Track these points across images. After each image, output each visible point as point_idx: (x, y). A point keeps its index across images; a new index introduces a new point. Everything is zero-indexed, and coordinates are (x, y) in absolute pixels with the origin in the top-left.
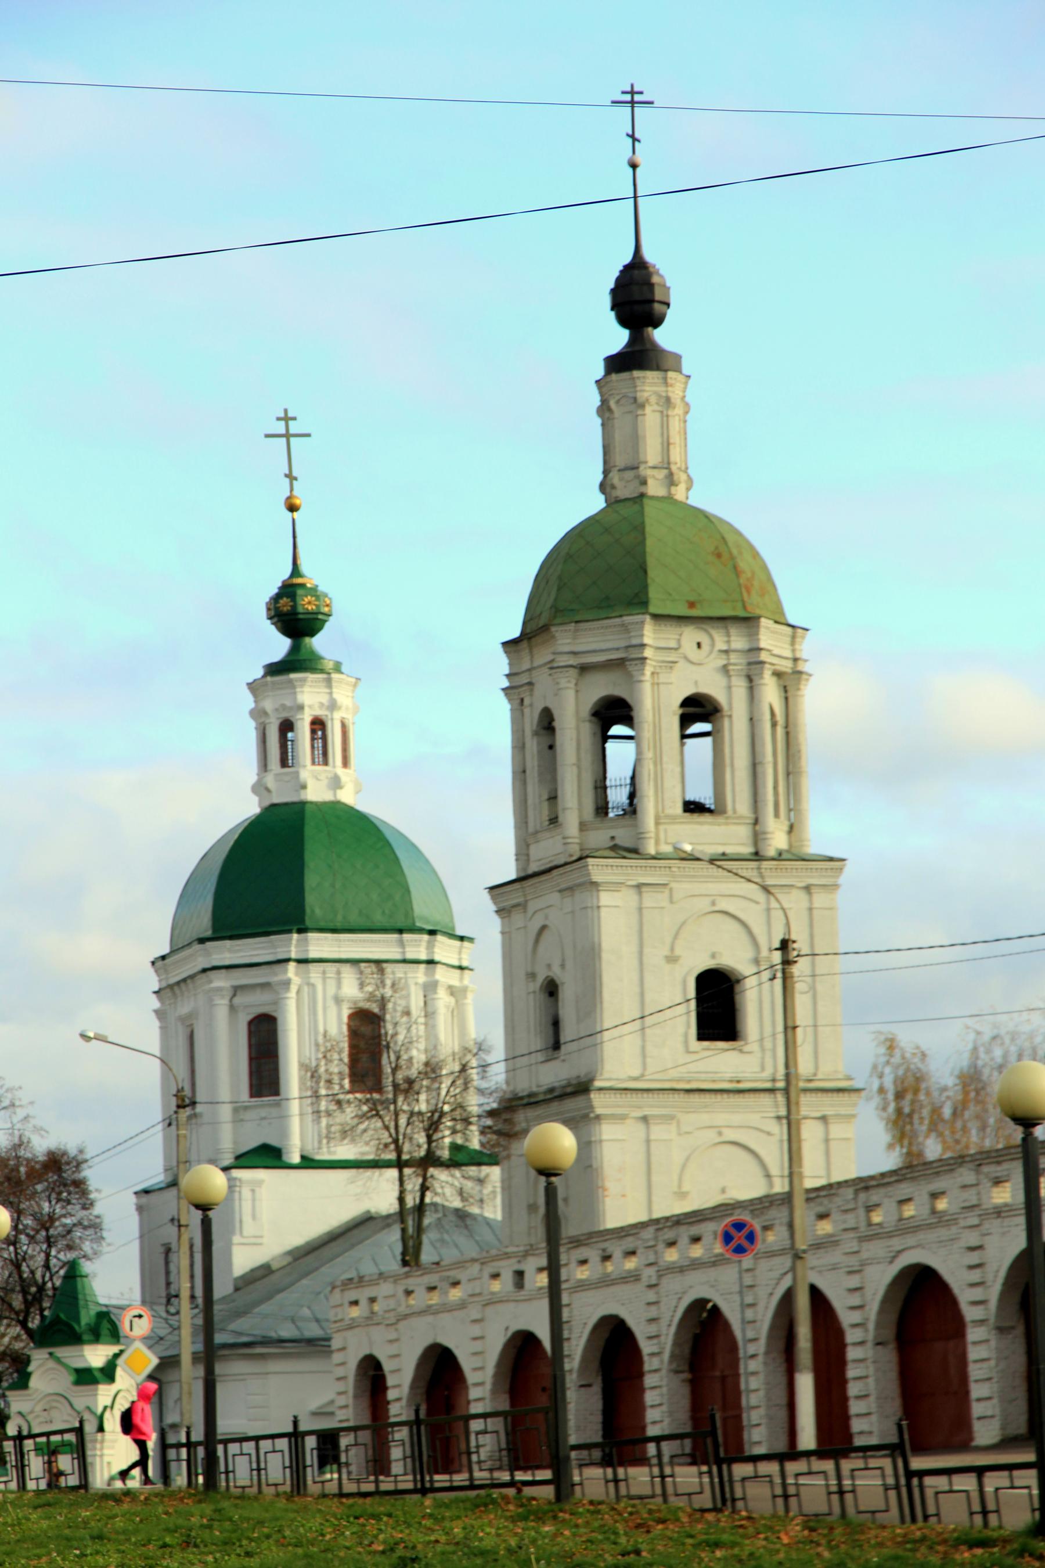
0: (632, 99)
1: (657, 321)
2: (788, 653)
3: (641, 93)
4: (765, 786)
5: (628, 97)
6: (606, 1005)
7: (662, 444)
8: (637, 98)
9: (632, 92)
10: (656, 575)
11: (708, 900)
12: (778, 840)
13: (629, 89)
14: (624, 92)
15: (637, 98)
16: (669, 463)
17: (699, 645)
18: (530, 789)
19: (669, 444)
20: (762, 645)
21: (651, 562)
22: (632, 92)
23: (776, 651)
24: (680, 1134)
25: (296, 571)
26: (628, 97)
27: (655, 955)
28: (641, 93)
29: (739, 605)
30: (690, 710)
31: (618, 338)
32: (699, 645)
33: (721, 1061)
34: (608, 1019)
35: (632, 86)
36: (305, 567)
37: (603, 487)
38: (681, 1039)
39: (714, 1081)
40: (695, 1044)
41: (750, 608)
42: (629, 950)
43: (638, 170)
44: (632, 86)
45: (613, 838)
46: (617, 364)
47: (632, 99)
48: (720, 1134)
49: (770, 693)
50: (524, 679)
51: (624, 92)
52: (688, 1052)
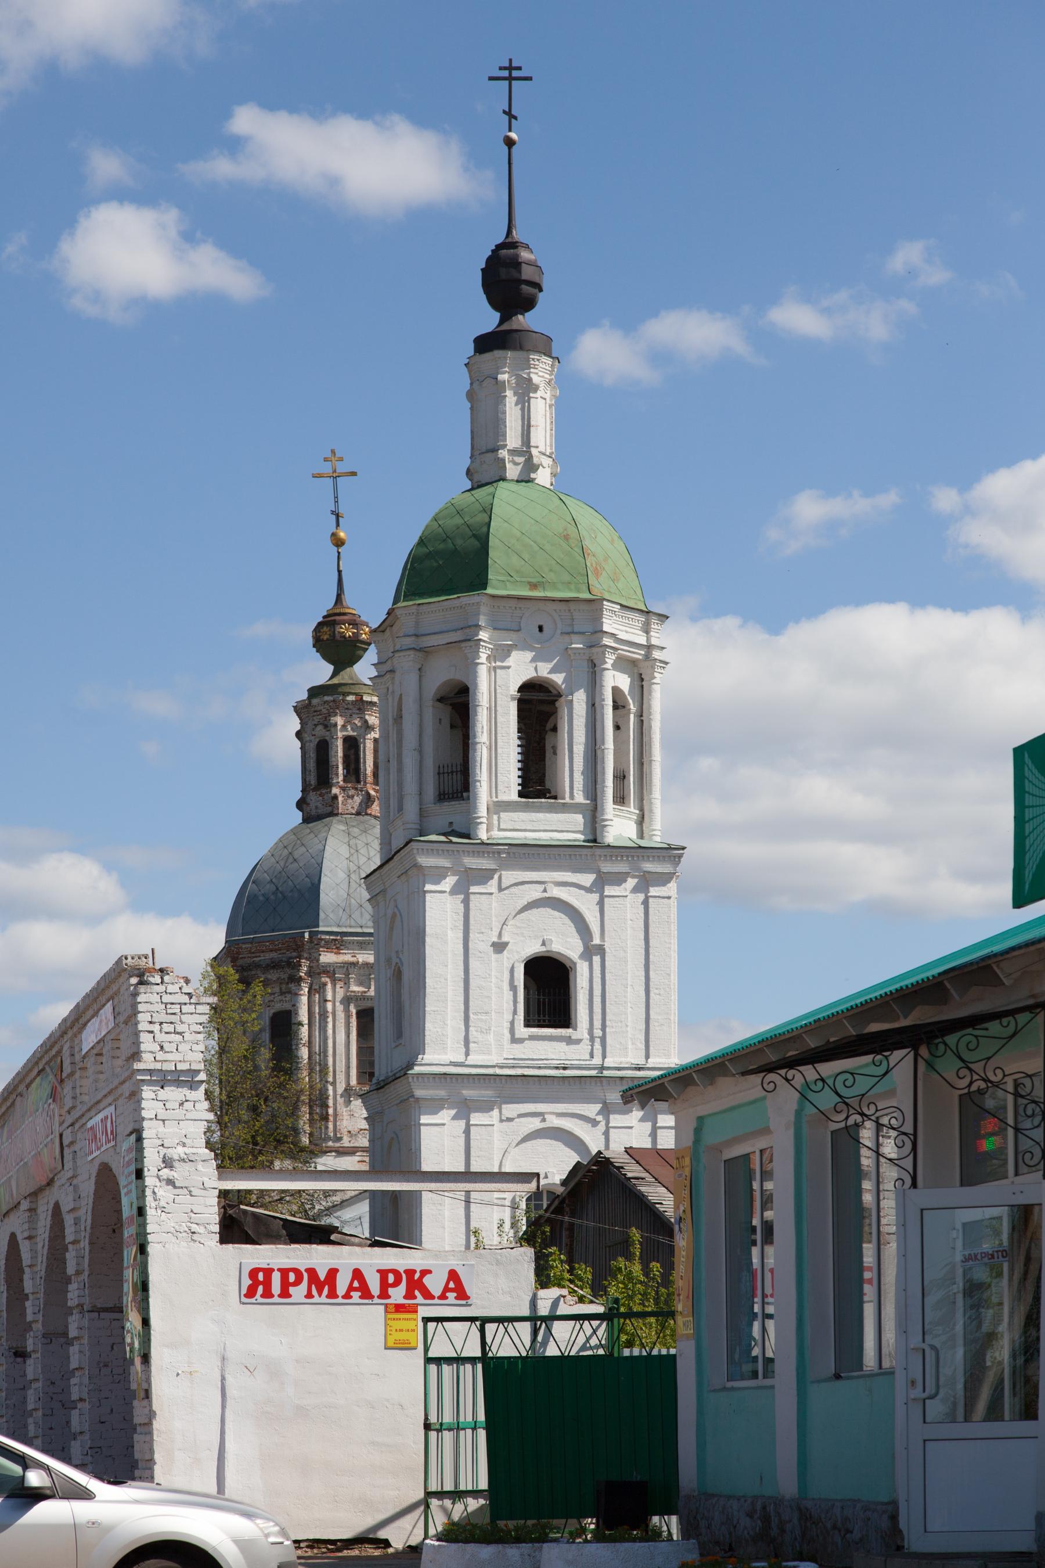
0: (511, 74)
1: (529, 304)
2: (642, 640)
3: (519, 68)
4: (604, 773)
5: (506, 73)
6: (429, 990)
7: (523, 426)
8: (515, 73)
9: (510, 68)
10: (496, 555)
11: (541, 887)
12: (620, 827)
13: (507, 65)
14: (501, 68)
15: (515, 73)
16: (529, 446)
17: (541, 629)
18: (391, 776)
19: (529, 426)
20: (606, 628)
21: (493, 542)
22: (510, 68)
23: (622, 636)
24: (501, 1121)
25: (509, 232)
26: (506, 73)
27: (480, 943)
28: (519, 68)
29: (585, 588)
30: (529, 696)
31: (489, 320)
32: (541, 629)
33: (548, 1050)
34: (818, 1066)
35: (511, 60)
36: (349, 599)
37: (469, 473)
38: (507, 1025)
39: (540, 1068)
40: (522, 1031)
41: (594, 591)
42: (455, 937)
43: (514, 149)
44: (511, 60)
45: (451, 823)
46: (485, 344)
47: (511, 74)
48: (544, 1120)
49: (615, 679)
50: (387, 667)
51: (501, 68)
52: (514, 1040)
